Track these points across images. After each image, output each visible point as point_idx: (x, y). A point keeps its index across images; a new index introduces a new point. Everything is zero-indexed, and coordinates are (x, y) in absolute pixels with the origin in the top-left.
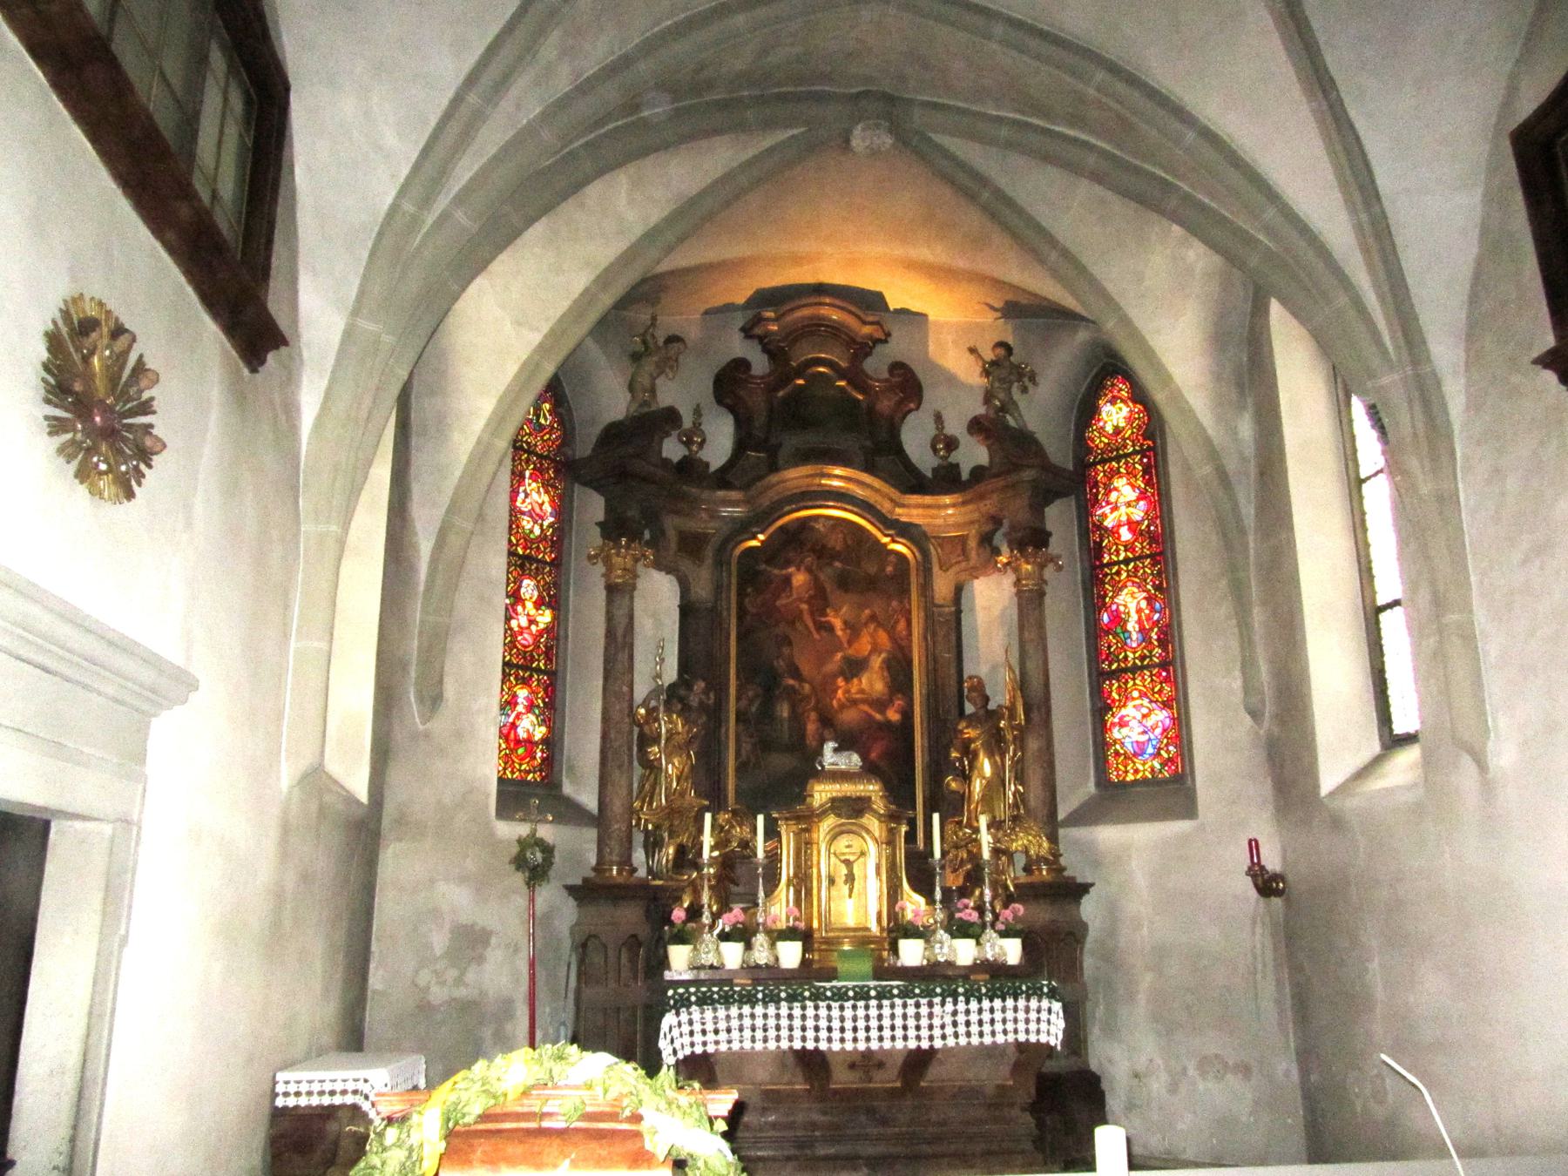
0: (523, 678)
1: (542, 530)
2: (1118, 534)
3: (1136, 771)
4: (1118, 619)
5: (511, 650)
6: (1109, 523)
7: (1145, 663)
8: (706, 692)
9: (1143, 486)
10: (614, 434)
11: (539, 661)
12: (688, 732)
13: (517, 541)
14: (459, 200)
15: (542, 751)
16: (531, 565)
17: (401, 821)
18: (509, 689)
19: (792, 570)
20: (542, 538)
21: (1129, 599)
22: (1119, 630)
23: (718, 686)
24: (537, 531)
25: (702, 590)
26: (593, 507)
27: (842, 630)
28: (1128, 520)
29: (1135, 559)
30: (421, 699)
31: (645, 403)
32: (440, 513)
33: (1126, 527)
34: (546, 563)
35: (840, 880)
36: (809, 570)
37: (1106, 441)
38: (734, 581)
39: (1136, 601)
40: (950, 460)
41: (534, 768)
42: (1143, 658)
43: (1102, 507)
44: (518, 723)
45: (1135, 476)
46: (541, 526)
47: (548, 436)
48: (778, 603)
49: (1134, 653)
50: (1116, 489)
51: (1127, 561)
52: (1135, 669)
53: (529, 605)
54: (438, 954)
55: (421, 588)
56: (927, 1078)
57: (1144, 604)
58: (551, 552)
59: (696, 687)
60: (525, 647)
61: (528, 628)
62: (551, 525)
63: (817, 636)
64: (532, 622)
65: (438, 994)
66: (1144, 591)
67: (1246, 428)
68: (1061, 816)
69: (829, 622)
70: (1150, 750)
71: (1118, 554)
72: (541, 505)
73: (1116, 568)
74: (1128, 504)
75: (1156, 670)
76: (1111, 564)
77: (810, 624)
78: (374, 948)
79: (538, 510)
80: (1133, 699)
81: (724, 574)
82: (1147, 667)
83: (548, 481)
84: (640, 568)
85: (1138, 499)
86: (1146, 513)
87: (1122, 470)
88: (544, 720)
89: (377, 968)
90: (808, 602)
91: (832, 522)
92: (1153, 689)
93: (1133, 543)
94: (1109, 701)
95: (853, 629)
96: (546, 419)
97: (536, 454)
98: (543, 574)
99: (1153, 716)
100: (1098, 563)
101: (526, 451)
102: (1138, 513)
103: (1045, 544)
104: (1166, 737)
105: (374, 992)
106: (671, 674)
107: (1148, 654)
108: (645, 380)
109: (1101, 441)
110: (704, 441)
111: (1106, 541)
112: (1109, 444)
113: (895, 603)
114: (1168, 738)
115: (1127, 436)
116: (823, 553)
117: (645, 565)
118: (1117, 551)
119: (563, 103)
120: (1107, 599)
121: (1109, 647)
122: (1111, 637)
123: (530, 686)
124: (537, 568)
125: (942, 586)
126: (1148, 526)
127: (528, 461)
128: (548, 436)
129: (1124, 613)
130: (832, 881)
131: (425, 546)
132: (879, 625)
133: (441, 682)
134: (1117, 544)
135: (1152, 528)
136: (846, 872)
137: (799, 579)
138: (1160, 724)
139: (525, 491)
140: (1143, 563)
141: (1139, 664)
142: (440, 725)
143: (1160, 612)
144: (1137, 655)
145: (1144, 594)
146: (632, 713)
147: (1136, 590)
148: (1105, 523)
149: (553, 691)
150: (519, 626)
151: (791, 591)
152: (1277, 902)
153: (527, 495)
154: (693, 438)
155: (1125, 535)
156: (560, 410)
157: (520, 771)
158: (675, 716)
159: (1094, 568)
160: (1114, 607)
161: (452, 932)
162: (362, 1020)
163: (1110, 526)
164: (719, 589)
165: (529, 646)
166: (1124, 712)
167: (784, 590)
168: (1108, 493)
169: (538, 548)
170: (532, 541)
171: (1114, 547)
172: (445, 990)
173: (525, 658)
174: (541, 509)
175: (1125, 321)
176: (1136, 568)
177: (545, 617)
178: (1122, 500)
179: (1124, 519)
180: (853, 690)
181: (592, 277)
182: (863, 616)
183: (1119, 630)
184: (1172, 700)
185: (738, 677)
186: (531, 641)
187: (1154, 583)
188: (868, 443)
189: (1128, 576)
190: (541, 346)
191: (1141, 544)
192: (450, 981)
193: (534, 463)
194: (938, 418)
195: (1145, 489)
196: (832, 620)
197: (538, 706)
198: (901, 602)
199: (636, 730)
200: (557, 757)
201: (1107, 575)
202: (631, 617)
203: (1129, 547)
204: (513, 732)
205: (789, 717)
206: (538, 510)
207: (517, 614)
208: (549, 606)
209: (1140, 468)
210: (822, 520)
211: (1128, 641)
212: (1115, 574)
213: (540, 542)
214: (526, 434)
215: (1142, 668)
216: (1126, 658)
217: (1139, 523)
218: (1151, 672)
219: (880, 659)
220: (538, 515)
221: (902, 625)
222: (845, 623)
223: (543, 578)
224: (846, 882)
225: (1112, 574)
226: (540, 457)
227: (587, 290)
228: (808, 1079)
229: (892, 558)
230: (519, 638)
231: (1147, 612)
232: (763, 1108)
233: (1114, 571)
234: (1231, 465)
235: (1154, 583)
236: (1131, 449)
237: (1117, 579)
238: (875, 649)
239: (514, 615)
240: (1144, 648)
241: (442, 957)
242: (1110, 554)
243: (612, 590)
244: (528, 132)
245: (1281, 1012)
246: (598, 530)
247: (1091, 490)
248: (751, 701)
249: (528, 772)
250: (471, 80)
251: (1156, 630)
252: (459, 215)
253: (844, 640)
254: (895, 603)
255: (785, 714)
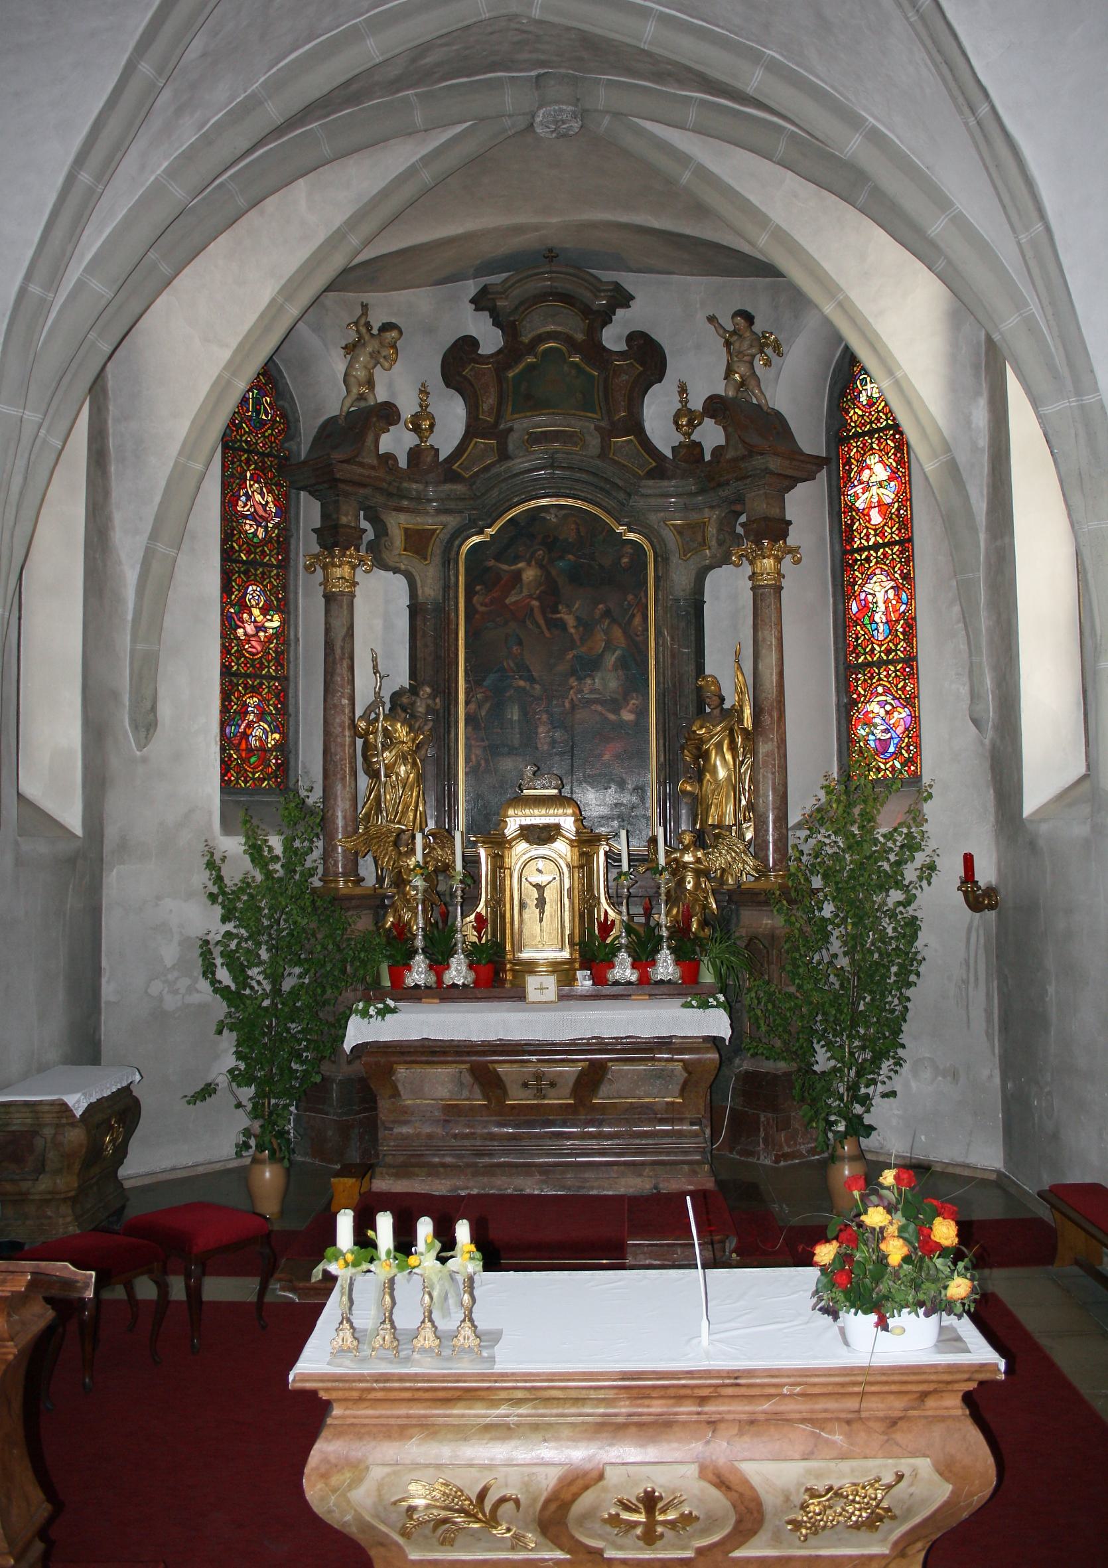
0: (253, 686)
1: (266, 531)
2: (869, 516)
3: (879, 770)
4: (866, 608)
5: (238, 659)
6: (860, 504)
7: (891, 657)
8: (433, 696)
9: (894, 464)
10: (331, 432)
11: (269, 667)
12: (413, 740)
13: (240, 546)
14: (91, 268)
15: (276, 758)
16: (256, 570)
17: (123, 846)
18: (238, 699)
19: (521, 565)
20: (267, 541)
21: (877, 588)
22: (867, 621)
23: (447, 692)
24: (261, 533)
25: (430, 591)
26: (310, 511)
27: (575, 627)
28: (878, 502)
29: (884, 545)
30: (135, 727)
31: (361, 397)
32: (142, 540)
33: (877, 509)
34: (272, 566)
35: (531, 902)
36: (541, 566)
37: (860, 413)
38: (462, 579)
39: (884, 590)
40: (693, 438)
41: (268, 775)
42: (888, 651)
43: (855, 486)
44: (249, 732)
45: (887, 454)
46: (267, 527)
47: (269, 432)
48: (507, 601)
49: (880, 646)
50: (869, 467)
51: (876, 547)
52: (881, 663)
53: (256, 612)
54: (169, 966)
55: (130, 617)
56: (601, 1094)
57: (891, 594)
58: (278, 554)
59: (422, 693)
60: (253, 654)
61: (256, 635)
62: (276, 526)
63: (547, 634)
64: (260, 628)
65: (171, 1003)
66: (891, 580)
67: (980, 416)
68: (790, 825)
69: (561, 619)
70: (892, 749)
71: (868, 540)
72: (264, 506)
73: (866, 553)
74: (880, 484)
75: (901, 665)
76: (861, 550)
77: (542, 622)
78: (104, 964)
79: (261, 512)
80: (879, 695)
81: (452, 572)
82: (892, 662)
83: (271, 479)
84: (360, 575)
85: (890, 479)
86: (896, 495)
87: (875, 446)
88: (277, 727)
89: (108, 982)
90: (538, 598)
91: (564, 512)
92: (896, 686)
93: (883, 527)
94: (855, 696)
95: (586, 626)
96: (267, 415)
97: (257, 453)
98: (270, 577)
99: (896, 714)
100: (848, 547)
101: (245, 451)
102: (888, 495)
103: (784, 535)
104: (908, 736)
105: (108, 1003)
106: (401, 678)
107: (893, 648)
108: (360, 374)
109: (855, 413)
110: (432, 426)
111: (857, 524)
112: (862, 416)
113: (630, 597)
114: (909, 738)
115: (880, 409)
116: (552, 544)
117: (366, 572)
118: (867, 535)
119: (189, 156)
120: (856, 587)
121: (857, 639)
122: (859, 628)
123: (260, 694)
124: (263, 573)
125: (681, 577)
126: (898, 510)
127: (248, 462)
128: (269, 432)
129: (873, 603)
130: (522, 905)
131: (130, 575)
132: (614, 621)
133: (154, 709)
134: (867, 528)
135: (902, 512)
136: (537, 896)
137: (530, 575)
138: (902, 722)
139: (246, 494)
140: (892, 550)
141: (885, 658)
142: (159, 746)
143: (907, 604)
144: (883, 648)
145: (892, 584)
146: (353, 726)
147: (884, 579)
148: (857, 504)
149: (286, 696)
150: (246, 634)
151: (521, 588)
152: (991, 915)
153: (248, 498)
154: (421, 423)
155: (876, 518)
156: (280, 403)
157: (253, 779)
158: (399, 725)
159: (845, 552)
160: (863, 596)
161: (180, 944)
162: (97, 1028)
163: (861, 507)
164: (448, 588)
165: (258, 653)
166: (869, 708)
167: (514, 588)
168: (860, 472)
169: (263, 551)
170: (256, 547)
171: (865, 531)
172: (179, 997)
173: (253, 666)
174: (265, 510)
175: (845, 306)
176: (884, 554)
177: (275, 623)
178: (873, 479)
179: (875, 500)
180: (586, 690)
181: (277, 288)
182: (597, 612)
183: (867, 621)
184: (914, 698)
185: (467, 681)
186: (259, 649)
187: (902, 571)
188: (602, 424)
189: (877, 563)
190: (230, 362)
191: (891, 529)
192: (182, 991)
193: (256, 463)
194: (683, 389)
195: (896, 468)
196: (566, 617)
197: (270, 714)
198: (636, 596)
199: (360, 742)
200: (292, 763)
201: (856, 561)
202: (351, 627)
203: (879, 532)
204: (244, 741)
205: (519, 721)
206: (261, 512)
207: (243, 622)
208: (278, 611)
209: (892, 445)
210: (552, 510)
211: (875, 633)
212: (864, 560)
213: (266, 545)
214: (246, 432)
215: (888, 662)
216: (873, 649)
217: (890, 505)
218: (895, 667)
219: (613, 659)
220: (261, 517)
221: (637, 620)
222: (578, 619)
223: (270, 582)
224: (537, 906)
225: (861, 560)
226: (263, 455)
227: (273, 300)
228: (486, 1097)
229: (628, 549)
230: (247, 646)
231: (894, 602)
232: (446, 1121)
233: (863, 557)
234: (962, 459)
235: (902, 571)
236: (884, 423)
237: (867, 565)
238: (609, 646)
239: (240, 624)
240: (890, 641)
241: (173, 967)
242: (860, 539)
243: (329, 598)
244: (157, 191)
245: (989, 1019)
246: (315, 536)
247: (843, 468)
248: (480, 706)
249: (264, 780)
250: (80, 160)
251: (902, 622)
252: (95, 285)
253: (576, 637)
254: (630, 597)
255: (515, 718)
